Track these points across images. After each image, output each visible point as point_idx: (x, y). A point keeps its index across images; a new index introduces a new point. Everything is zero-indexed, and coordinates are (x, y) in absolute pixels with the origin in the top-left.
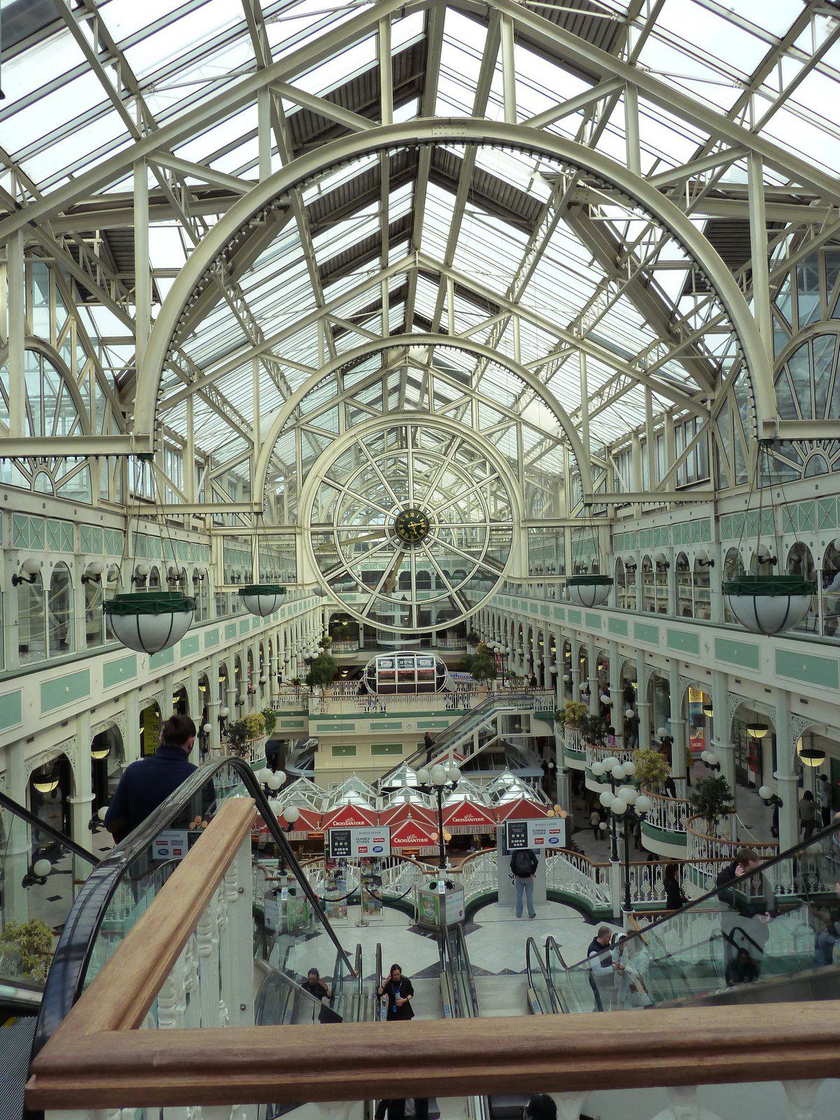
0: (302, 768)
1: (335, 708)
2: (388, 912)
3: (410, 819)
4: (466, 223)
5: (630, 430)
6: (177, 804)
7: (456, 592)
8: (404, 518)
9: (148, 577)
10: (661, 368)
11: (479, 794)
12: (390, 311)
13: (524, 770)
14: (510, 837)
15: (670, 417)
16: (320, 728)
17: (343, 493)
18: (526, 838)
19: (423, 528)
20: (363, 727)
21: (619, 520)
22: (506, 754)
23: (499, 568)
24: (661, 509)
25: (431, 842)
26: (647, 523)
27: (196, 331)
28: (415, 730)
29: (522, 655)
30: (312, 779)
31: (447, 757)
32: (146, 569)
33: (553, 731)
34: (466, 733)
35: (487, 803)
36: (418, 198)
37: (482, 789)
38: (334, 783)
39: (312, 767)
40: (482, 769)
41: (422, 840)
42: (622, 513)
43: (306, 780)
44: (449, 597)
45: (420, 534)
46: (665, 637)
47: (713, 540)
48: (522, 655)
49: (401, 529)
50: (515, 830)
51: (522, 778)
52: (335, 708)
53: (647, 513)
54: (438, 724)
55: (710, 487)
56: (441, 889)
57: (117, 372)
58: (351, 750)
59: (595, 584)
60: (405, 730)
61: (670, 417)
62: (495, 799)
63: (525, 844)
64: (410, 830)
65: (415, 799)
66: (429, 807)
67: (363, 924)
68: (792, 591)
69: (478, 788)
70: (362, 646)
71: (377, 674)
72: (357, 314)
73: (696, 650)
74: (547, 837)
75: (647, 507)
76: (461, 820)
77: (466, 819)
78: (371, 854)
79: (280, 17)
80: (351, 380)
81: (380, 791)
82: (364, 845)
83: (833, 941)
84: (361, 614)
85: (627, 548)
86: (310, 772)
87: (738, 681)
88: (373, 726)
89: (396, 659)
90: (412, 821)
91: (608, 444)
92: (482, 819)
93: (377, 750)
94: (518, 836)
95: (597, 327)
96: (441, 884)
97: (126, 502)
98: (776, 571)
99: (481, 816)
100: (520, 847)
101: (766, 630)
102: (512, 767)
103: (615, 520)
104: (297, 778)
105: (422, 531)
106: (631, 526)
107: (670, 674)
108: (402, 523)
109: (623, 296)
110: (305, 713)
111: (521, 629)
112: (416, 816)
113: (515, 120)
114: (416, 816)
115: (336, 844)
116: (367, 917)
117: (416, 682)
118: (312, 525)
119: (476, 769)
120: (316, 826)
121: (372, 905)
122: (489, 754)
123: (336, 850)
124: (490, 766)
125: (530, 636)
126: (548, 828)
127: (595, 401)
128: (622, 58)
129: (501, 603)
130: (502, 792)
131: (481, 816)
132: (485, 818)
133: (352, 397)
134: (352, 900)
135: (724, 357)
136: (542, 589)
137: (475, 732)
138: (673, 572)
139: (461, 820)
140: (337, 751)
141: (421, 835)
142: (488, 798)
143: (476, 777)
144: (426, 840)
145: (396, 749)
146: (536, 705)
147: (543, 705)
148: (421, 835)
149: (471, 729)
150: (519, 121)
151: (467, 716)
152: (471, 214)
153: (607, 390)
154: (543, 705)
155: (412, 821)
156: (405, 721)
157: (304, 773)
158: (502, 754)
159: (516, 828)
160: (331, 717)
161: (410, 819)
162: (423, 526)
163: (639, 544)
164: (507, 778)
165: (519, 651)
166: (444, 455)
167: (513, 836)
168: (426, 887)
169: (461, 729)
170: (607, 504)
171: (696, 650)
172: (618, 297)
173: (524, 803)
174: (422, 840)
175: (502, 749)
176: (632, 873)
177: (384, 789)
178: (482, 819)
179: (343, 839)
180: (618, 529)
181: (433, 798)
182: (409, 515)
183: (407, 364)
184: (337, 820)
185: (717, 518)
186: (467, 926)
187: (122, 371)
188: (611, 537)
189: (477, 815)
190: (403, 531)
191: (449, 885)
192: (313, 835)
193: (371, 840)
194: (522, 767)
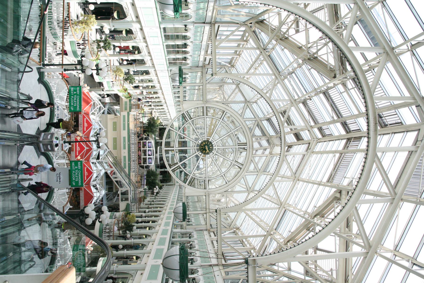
0: (108, 109)
3: (86, 148)
4: (331, 155)
5: (255, 246)
7: (179, 166)
8: (210, 144)
9: (186, 62)
10: (274, 240)
11: (96, 180)
12: (292, 135)
13: (106, 199)
15: (252, 249)
16: (124, 116)
17: (219, 120)
19: (205, 152)
21: (209, 233)
22: (112, 193)
23: (189, 184)
24: (214, 247)
25: (76, 156)
26: (208, 242)
27: (286, 50)
28: (123, 155)
29: (145, 212)
30: (103, 113)
31: (111, 167)
32: (188, 49)
33: (122, 211)
35: (92, 183)
36: (339, 138)
37: (99, 182)
39: (109, 113)
40: (106, 182)
41: (77, 153)
42: (212, 234)
43: (103, 110)
44: (177, 163)
45: (203, 151)
46: (160, 246)
47: (202, 264)
49: (205, 143)
51: (102, 199)
53: (213, 243)
55: (223, 262)
57: (268, 20)
58: (115, 129)
59: (180, 270)
60: (123, 151)
61: (252, 249)
64: (82, 148)
65: (95, 153)
66: (91, 158)
68: (182, 270)
69: (99, 180)
70: (157, 141)
71: (146, 141)
72: (292, 121)
73: (155, 258)
75: (215, 243)
76: (85, 171)
80: (266, 124)
84: (170, 127)
85: (197, 235)
86: (106, 112)
87: (142, 274)
88: (125, 157)
89: (152, 157)
90: (85, 149)
91: (240, 228)
93: (115, 140)
95: (290, 213)
96: (58, 142)
97: (217, 23)
98: (189, 264)
99: (87, 130)
101: (164, 261)
102: (107, 195)
103: (209, 232)
105: (204, 151)
106: (207, 237)
107: (145, 250)
108: (208, 143)
109: (304, 220)
111: (156, 216)
112: (88, 151)
113: (379, 152)
114: (88, 151)
118: (207, 107)
120: (85, 185)
122: (112, 185)
125: (160, 208)
127: (258, 219)
129: (174, 202)
130: (97, 189)
131: (87, 130)
132: (86, 180)
133: (258, 125)
135: (278, 266)
136: (189, 77)
139: (85, 171)
140: (115, 124)
141: (80, 152)
142: (94, 183)
143: (103, 179)
144: (77, 154)
145: (115, 148)
146: (133, 204)
147: (132, 207)
148: (80, 152)
150: (379, 154)
152: (335, 156)
153: (263, 223)
154: (132, 207)
155: (85, 149)
156: (126, 151)
157: (106, 109)
161: (86, 148)
162: (206, 152)
163: (199, 239)
164: (103, 192)
166: (235, 161)
169: (123, 174)
170: (217, 228)
171: (155, 258)
172: (303, 217)
173: (92, 197)
174: (77, 153)
175: (114, 191)
178: (86, 179)
180: (206, 233)
181: (94, 139)
182: (211, 146)
183: (272, 146)
184: (87, 119)
185: (211, 265)
186: (39, 153)
187: (269, 22)
188: (202, 230)
189: (88, 177)
190: (204, 144)
194: (107, 199)
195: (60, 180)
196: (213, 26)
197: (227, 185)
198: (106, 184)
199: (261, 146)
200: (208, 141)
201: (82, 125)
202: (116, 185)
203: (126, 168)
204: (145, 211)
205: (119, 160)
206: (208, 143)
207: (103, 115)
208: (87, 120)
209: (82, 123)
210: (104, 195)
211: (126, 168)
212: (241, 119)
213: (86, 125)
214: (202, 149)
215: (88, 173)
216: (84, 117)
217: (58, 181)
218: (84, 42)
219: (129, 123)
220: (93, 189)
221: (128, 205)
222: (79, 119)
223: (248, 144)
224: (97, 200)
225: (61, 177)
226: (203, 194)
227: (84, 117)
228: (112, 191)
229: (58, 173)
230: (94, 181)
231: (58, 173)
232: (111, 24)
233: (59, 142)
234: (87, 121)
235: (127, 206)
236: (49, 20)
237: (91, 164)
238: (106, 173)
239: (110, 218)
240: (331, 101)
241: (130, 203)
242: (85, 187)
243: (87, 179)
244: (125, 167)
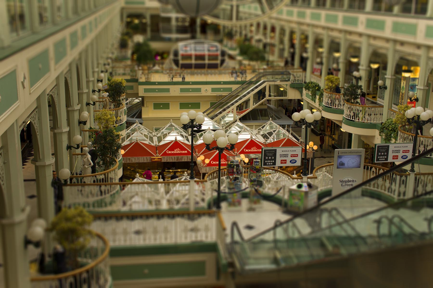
1: (156, 78)
2: (266, 204)
6: (183, 131)
14: (378, 154)
16: (146, 90)
18: (275, 159)
20: (175, 91)
28: (210, 93)
33: (302, 96)
35: (155, 142)
38: (158, 127)
50: (268, 154)
52: (156, 78)
54: (225, 90)
56: (305, 188)
58: (166, 106)
60: (203, 93)
63: (387, 159)
67: (251, 209)
74: (289, 159)
77: (252, 150)
78: (288, 164)
82: (284, 159)
88: (213, 90)
92: (186, 152)
96: (305, 185)
99: (185, 150)
100: (383, 161)
104: (134, 123)
110: (136, 81)
115: (380, 154)
116: (254, 206)
117: (207, 62)
119: (250, 119)
121: (255, 199)
123: (266, 161)
124: (258, 118)
126: (290, 154)
132: (188, 151)
134: (245, 196)
140: (157, 106)
142: (155, 139)
145: (196, 106)
147: (296, 79)
151: (245, 86)
158: (265, 110)
159: (269, 153)
160: (154, 83)
167: (267, 158)
168: (294, 187)
178: (186, 152)
179: (271, 155)
191: (310, 186)
192: (155, 159)
193: (289, 156)
195: (350, 181)
201: (180, 156)
202: (260, 105)
203: (231, 88)
205: (218, 100)
208: (169, 149)
209: (176, 156)
210: (244, 125)
211: (231, 88)
213: (177, 151)
215: (177, 148)
216: (165, 154)
217: (353, 183)
219: (192, 82)
222: (169, 161)
224: (182, 136)
225: (346, 179)
227: (165, 154)
229: (341, 184)
231: (341, 184)
233: (305, 182)
234: (171, 149)
235: (294, 88)
236: (380, 188)
237: (162, 143)
241: (289, 83)
242: (199, 153)
243: (186, 150)
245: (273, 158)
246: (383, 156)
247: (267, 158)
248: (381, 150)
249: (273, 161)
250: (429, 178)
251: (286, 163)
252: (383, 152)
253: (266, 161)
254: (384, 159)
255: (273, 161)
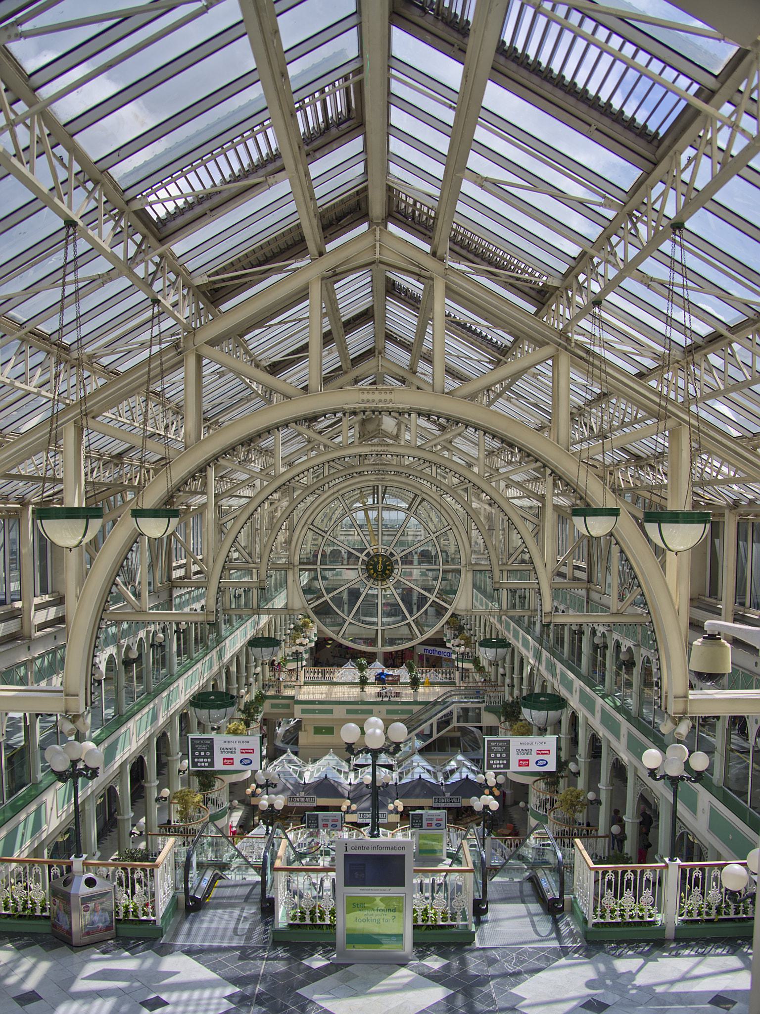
14: (489, 755)
16: (304, 711)
18: (212, 756)
29: (504, 675)
34: (426, 722)
39: (296, 742)
40: (440, 750)
48: (504, 675)
62: (446, 778)
63: (212, 764)
74: (533, 758)
79: (26, 27)
81: (352, 768)
83: (570, 713)
86: (295, 749)
94: (202, 754)
100: (205, 766)
102: (464, 752)
108: (371, 565)
126: (535, 748)
128: (558, 325)
130: (452, 772)
137: (434, 720)
138: (723, 726)
140: (318, 730)
142: (441, 778)
146: (486, 699)
149: (431, 718)
154: (492, 700)
159: (200, 744)
165: (501, 671)
175: (458, 734)
176: (629, 880)
177: (356, 765)
194: (473, 750)
196: (175, 584)
197: (454, 528)
198: (445, 751)
199: (365, 316)
200: (370, 577)
204: (502, 675)
206: (371, 565)
207: (299, 754)
212: (325, 496)
214: (382, 576)
218: (628, 886)
220: (451, 781)
221: (489, 709)
223: (376, 483)
226: (470, 575)
228: (458, 738)
230: (436, 777)
232: (175, 758)
238: (421, 751)
239: (399, 881)
240: (262, 172)
241: (484, 705)
244: (410, 711)
245: (504, 755)
246: (204, 757)
247: (493, 755)
248: (495, 749)
249: (505, 762)
250: (372, 899)
251: (232, 764)
252: (203, 751)
253: (196, 760)
254: (502, 766)
255: (505, 762)
